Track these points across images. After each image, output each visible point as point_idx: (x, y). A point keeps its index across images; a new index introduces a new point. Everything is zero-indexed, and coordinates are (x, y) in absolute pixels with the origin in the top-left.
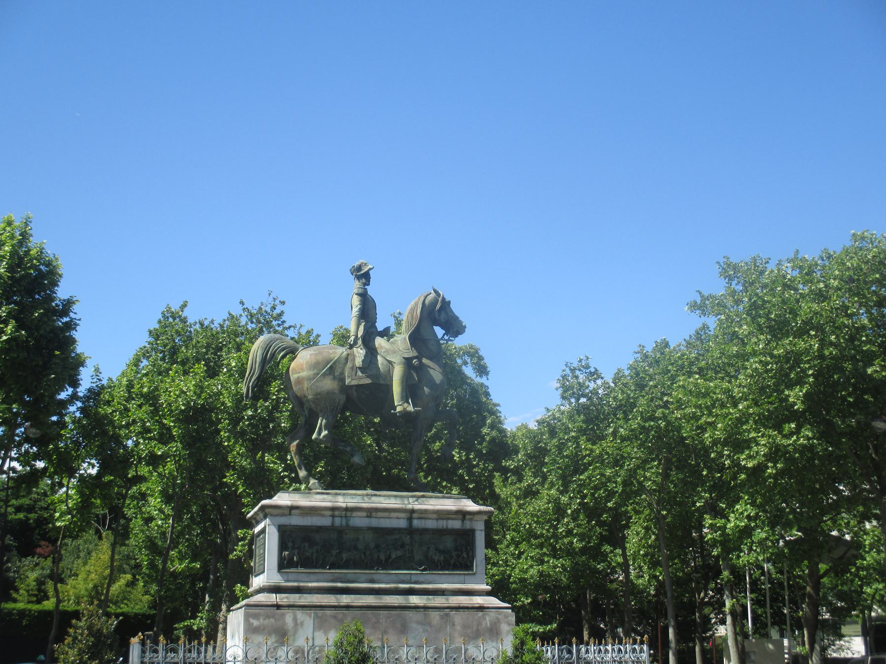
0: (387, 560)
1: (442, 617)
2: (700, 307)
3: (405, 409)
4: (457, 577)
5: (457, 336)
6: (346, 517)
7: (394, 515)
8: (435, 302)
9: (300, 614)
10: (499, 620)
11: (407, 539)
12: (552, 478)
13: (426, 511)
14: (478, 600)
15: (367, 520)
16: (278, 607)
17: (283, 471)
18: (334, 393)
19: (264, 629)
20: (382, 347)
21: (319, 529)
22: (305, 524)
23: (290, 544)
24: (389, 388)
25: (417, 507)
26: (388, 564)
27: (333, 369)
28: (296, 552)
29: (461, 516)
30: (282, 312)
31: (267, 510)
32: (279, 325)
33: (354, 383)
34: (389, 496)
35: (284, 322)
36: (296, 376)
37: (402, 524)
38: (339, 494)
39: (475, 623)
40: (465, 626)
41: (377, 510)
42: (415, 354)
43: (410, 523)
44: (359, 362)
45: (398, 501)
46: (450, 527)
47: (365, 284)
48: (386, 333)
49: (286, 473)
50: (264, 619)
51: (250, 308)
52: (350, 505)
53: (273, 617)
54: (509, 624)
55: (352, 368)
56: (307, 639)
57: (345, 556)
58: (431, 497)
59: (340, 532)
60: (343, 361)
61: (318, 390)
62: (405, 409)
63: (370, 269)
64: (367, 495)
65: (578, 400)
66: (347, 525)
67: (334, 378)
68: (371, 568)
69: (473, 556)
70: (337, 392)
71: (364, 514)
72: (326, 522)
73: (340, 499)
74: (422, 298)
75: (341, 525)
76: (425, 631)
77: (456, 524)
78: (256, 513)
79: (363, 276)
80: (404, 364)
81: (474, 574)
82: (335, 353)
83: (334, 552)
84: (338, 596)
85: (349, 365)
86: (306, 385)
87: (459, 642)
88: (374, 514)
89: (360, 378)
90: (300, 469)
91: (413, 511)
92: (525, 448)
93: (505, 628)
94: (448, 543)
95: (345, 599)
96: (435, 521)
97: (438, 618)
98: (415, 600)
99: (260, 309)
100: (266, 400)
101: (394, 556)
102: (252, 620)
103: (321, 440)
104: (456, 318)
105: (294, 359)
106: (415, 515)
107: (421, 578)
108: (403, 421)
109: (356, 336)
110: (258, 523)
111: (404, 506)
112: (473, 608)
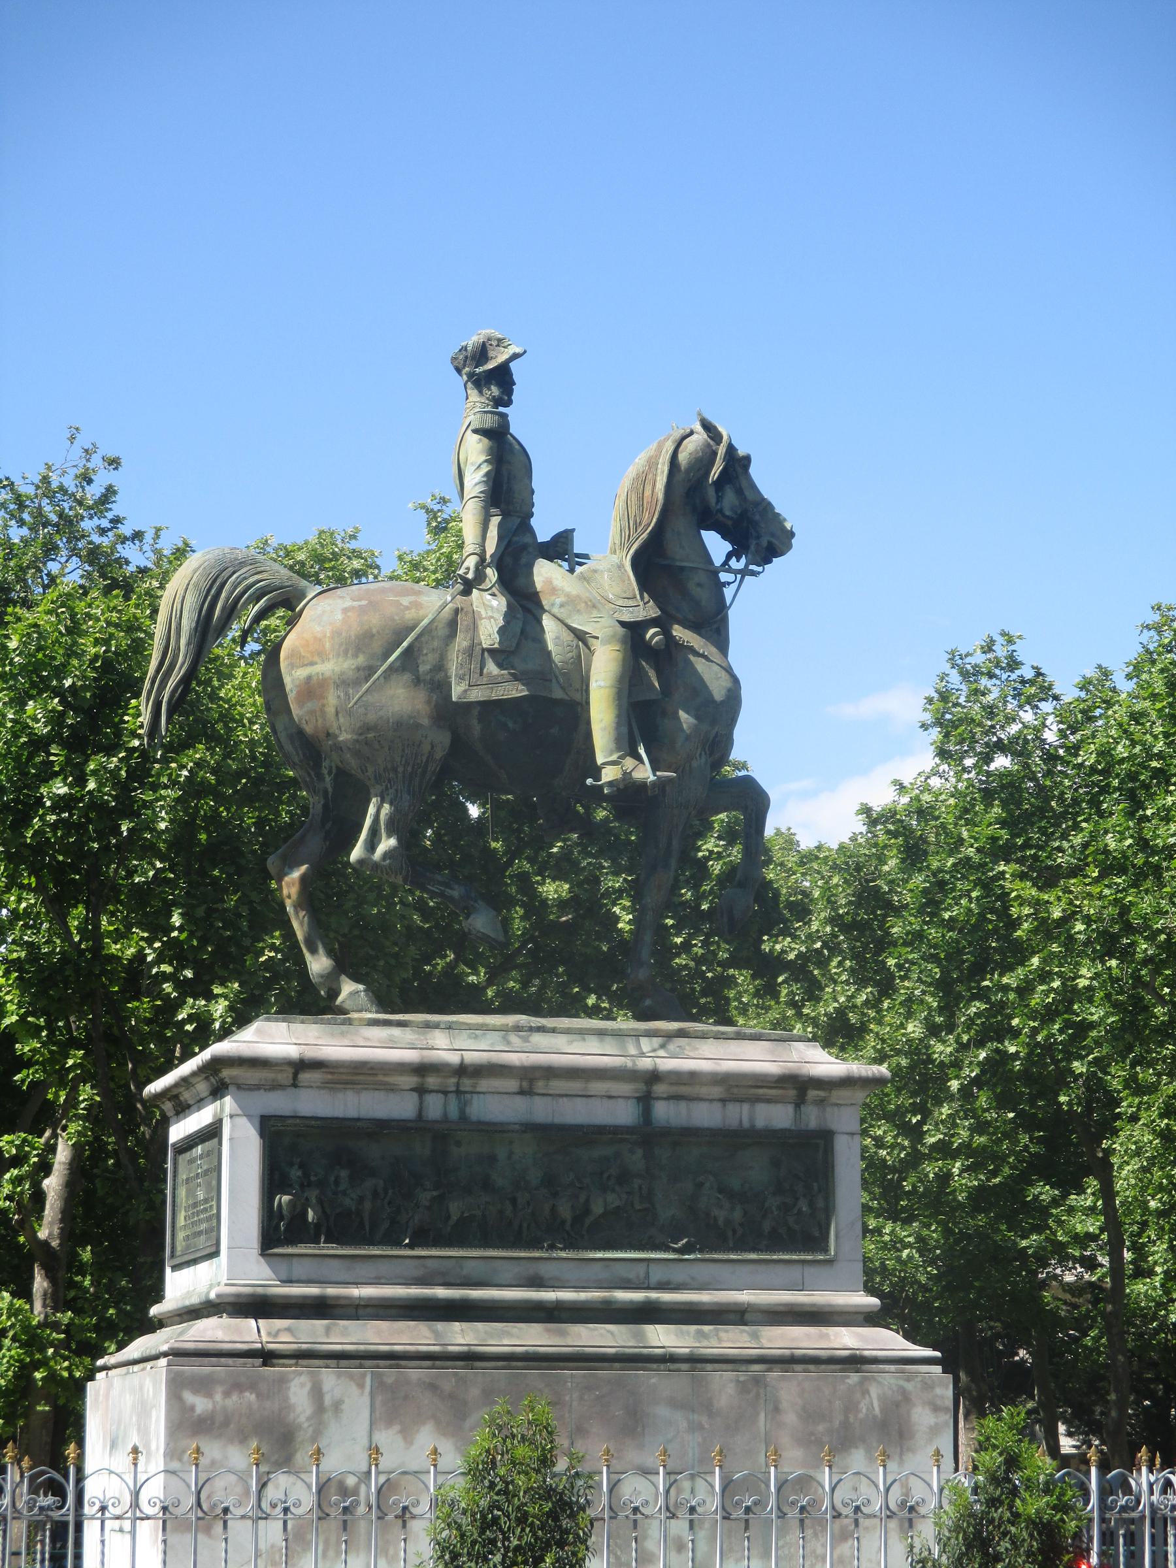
0: (578, 1219)
1: (743, 1387)
3: (626, 775)
4: (780, 1269)
5: (768, 561)
6: (458, 1092)
7: (598, 1087)
8: (705, 459)
9: (331, 1379)
10: (906, 1397)
11: (636, 1159)
12: (906, 987)
13: (693, 1077)
14: (846, 1339)
15: (520, 1103)
16: (267, 1357)
17: (159, 961)
18: (418, 726)
19: (226, 1423)
20: (554, 591)
21: (380, 1128)
22: (352, 1113)
23: (295, 1173)
24: (575, 713)
25: (667, 1064)
26: (581, 1232)
27: (410, 653)
28: (313, 1194)
29: (792, 1093)
30: (110, 492)
31: (226, 1073)
32: (103, 532)
33: (476, 695)
34: (582, 1033)
35: (116, 521)
36: (302, 673)
37: (624, 1114)
38: (436, 1026)
39: (838, 1404)
40: (810, 1415)
41: (550, 1072)
42: (652, 611)
43: (647, 1112)
44: (489, 632)
45: (610, 1046)
46: (760, 1123)
47: (498, 402)
48: (560, 548)
49: (166, 968)
50: (227, 1394)
51: (18, 482)
52: (471, 1057)
53: (252, 1387)
54: (936, 1409)
55: (470, 652)
56: (938, 1453)
57: (455, 1208)
58: (703, 1036)
59: (439, 1135)
60: (442, 631)
61: (372, 717)
62: (626, 775)
63: (515, 356)
64: (517, 1028)
65: (988, 759)
66: (463, 1117)
67: (417, 681)
68: (534, 1244)
69: (828, 1211)
70: (425, 722)
71: (512, 1085)
72: (401, 1107)
73: (439, 1039)
74: (669, 447)
75: (445, 1118)
76: (695, 1427)
77: (778, 1116)
78: (185, 1081)
79: (492, 377)
80: (623, 641)
81: (830, 1262)
82: (417, 605)
83: (425, 1197)
84: (440, 1326)
85: (462, 641)
86: (332, 699)
87: (794, 1462)
88: (540, 1086)
89: (494, 682)
90: (313, 951)
91: (654, 1077)
92: (831, 903)
93: (922, 1417)
94: (756, 1170)
95: (461, 1335)
96: (717, 1106)
97: (731, 1389)
98: (662, 1337)
99: (46, 480)
100: (110, 751)
101: (598, 1209)
102: (189, 1397)
103: (376, 866)
104: (765, 507)
105: (291, 622)
106: (660, 1089)
107: (679, 1274)
108: (545, 808)
109: (482, 559)
110: (183, 1110)
111: (629, 1063)
112: (815, 1361)
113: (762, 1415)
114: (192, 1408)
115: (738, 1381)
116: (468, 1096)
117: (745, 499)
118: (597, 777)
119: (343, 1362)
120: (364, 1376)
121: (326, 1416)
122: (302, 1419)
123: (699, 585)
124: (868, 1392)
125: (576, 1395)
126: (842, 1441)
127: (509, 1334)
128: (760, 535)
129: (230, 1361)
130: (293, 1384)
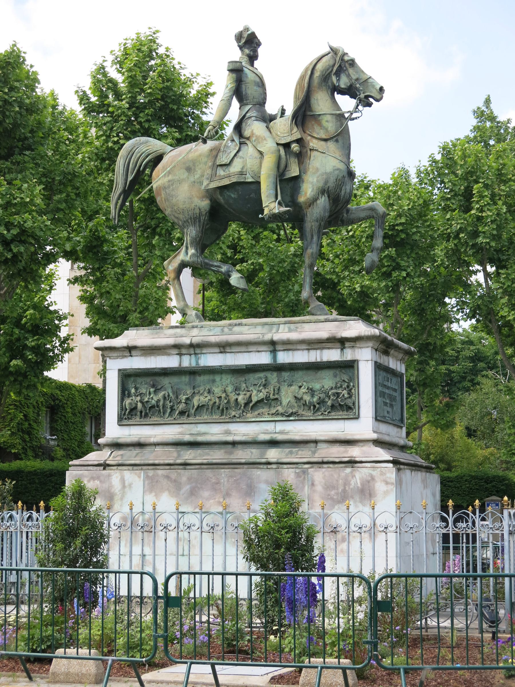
1: (298, 475)
2: (429, 161)
9: (129, 475)
10: (373, 478)
34: (256, 325)
40: (329, 487)
43: (275, 358)
46: (325, 359)
53: (98, 478)
93: (380, 487)
101: (255, 399)
113: (306, 487)
115: (295, 472)
116: (199, 355)
117: (351, 79)
119: (135, 468)
120: (141, 473)
121: (126, 490)
122: (117, 491)
123: (327, 121)
124: (355, 476)
125: (226, 480)
126: (344, 497)
127: (208, 454)
128: (365, 94)
129: (95, 468)
130: (113, 477)
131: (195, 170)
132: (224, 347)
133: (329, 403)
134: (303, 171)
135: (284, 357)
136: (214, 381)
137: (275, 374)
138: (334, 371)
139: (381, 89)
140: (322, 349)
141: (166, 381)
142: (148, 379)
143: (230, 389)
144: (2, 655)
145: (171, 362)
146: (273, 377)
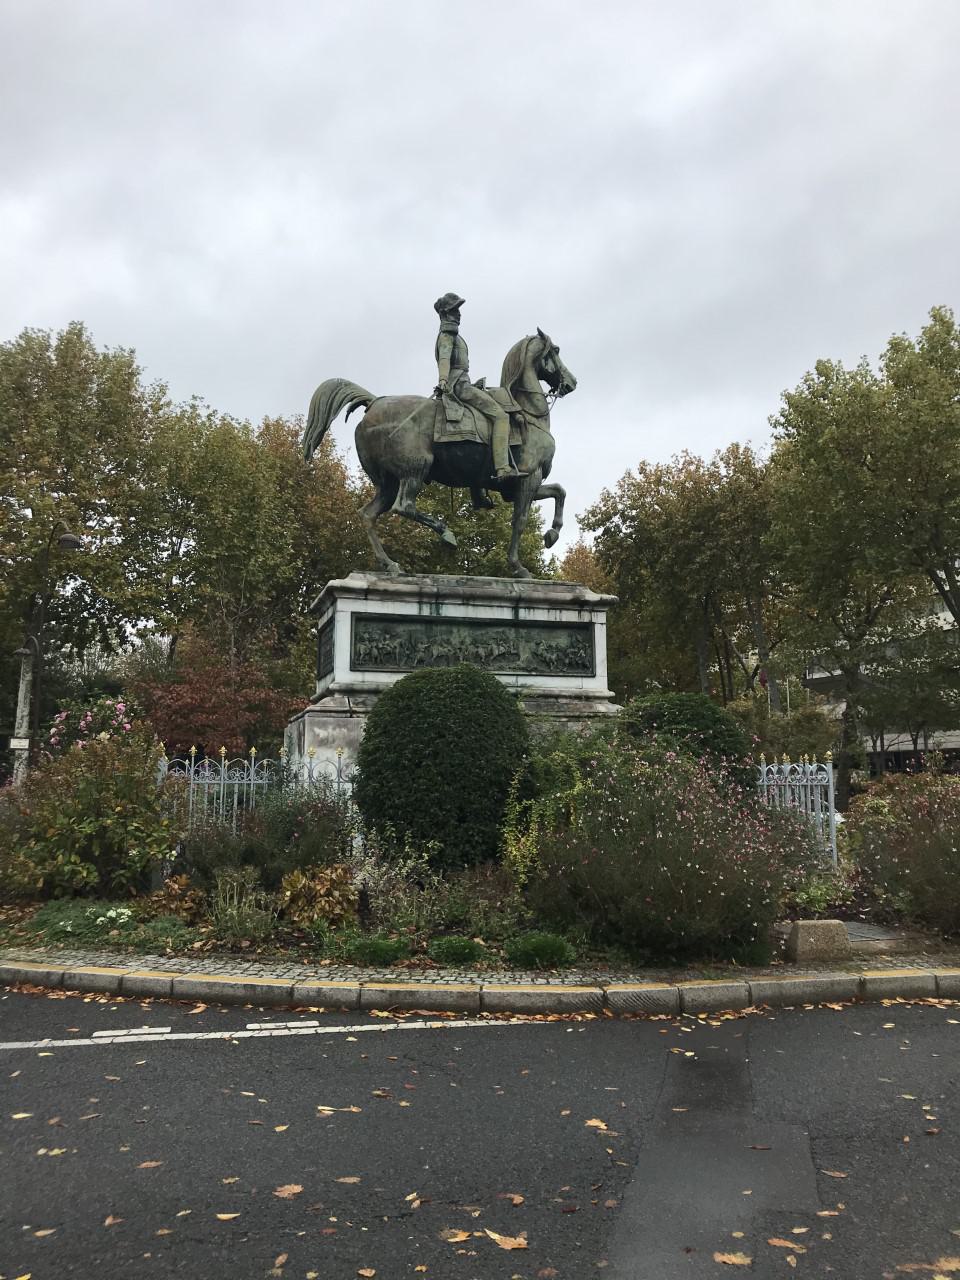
33: (444, 439)
43: (516, 614)
50: (334, 729)
53: (345, 726)
101: (496, 652)
114: (318, 735)
118: (496, 475)
128: (561, 384)
131: (421, 422)
132: (467, 600)
133: (567, 661)
134: (524, 442)
135: (524, 614)
136: (451, 632)
137: (513, 630)
138: (570, 631)
139: (575, 383)
140: (561, 610)
141: (401, 629)
142: (381, 626)
143: (468, 641)
144: (948, 726)
145: (410, 609)
146: (511, 633)
